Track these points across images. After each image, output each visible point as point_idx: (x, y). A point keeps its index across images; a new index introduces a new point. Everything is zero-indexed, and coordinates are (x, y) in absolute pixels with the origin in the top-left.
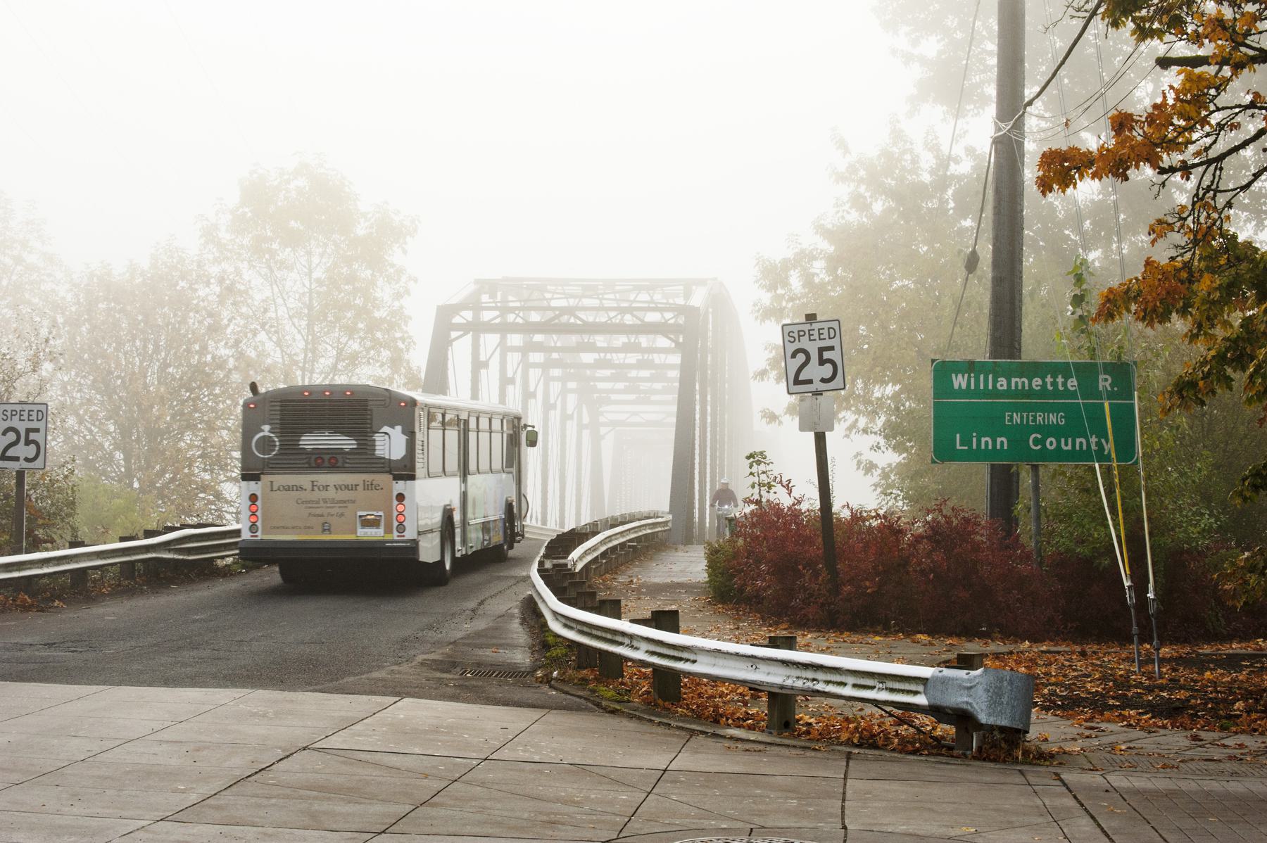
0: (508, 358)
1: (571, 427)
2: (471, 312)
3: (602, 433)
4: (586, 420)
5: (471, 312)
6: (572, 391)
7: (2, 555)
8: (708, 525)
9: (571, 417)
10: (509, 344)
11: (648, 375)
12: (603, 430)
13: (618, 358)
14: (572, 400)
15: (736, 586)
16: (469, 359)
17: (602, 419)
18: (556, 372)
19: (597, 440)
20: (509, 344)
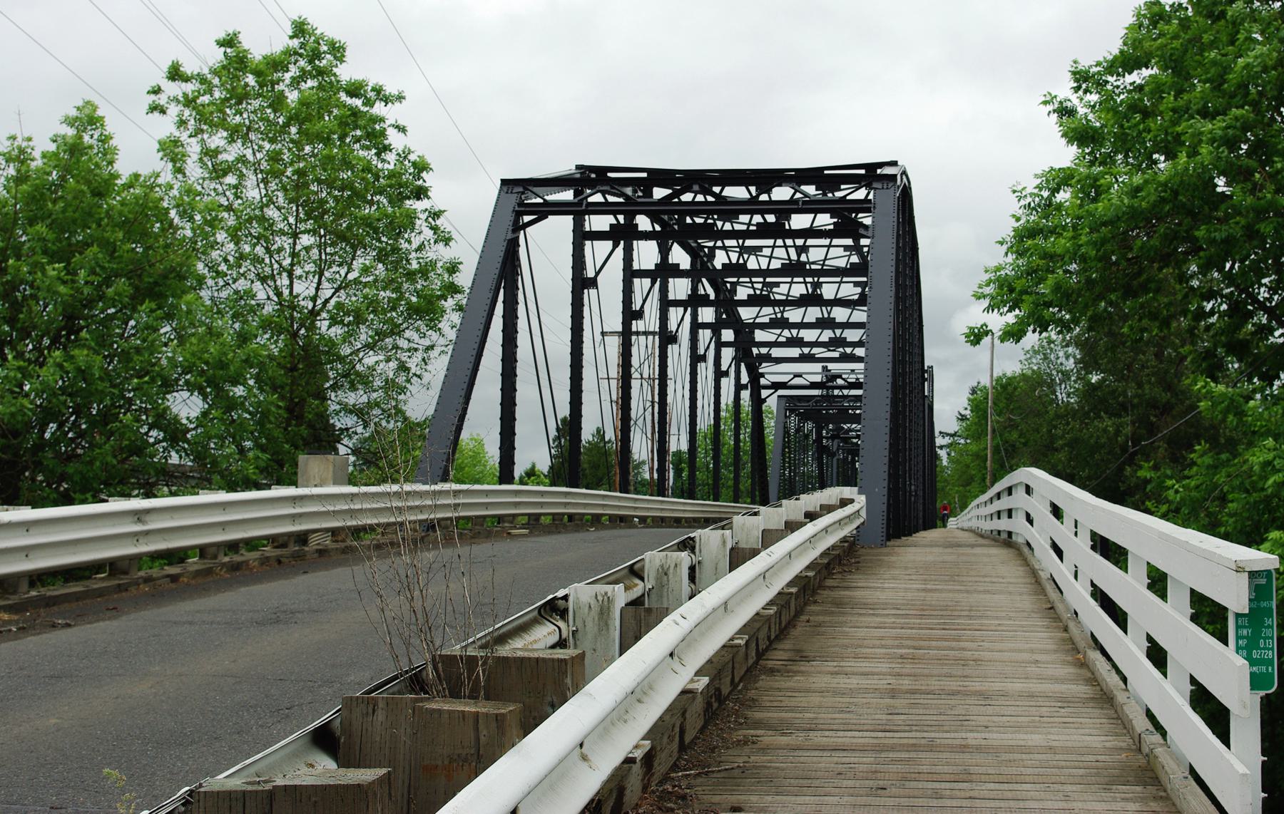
0: (586, 248)
1: (679, 355)
2: (571, 217)
3: (763, 397)
4: (745, 379)
5: (571, 217)
6: (727, 344)
7: (12, 499)
8: (671, 484)
9: (726, 374)
10: (700, 321)
11: (741, 216)
12: (764, 393)
13: (809, 335)
14: (728, 354)
15: (1126, 201)
16: (568, 274)
17: (763, 381)
18: (601, 223)
19: (758, 401)
20: (700, 321)
